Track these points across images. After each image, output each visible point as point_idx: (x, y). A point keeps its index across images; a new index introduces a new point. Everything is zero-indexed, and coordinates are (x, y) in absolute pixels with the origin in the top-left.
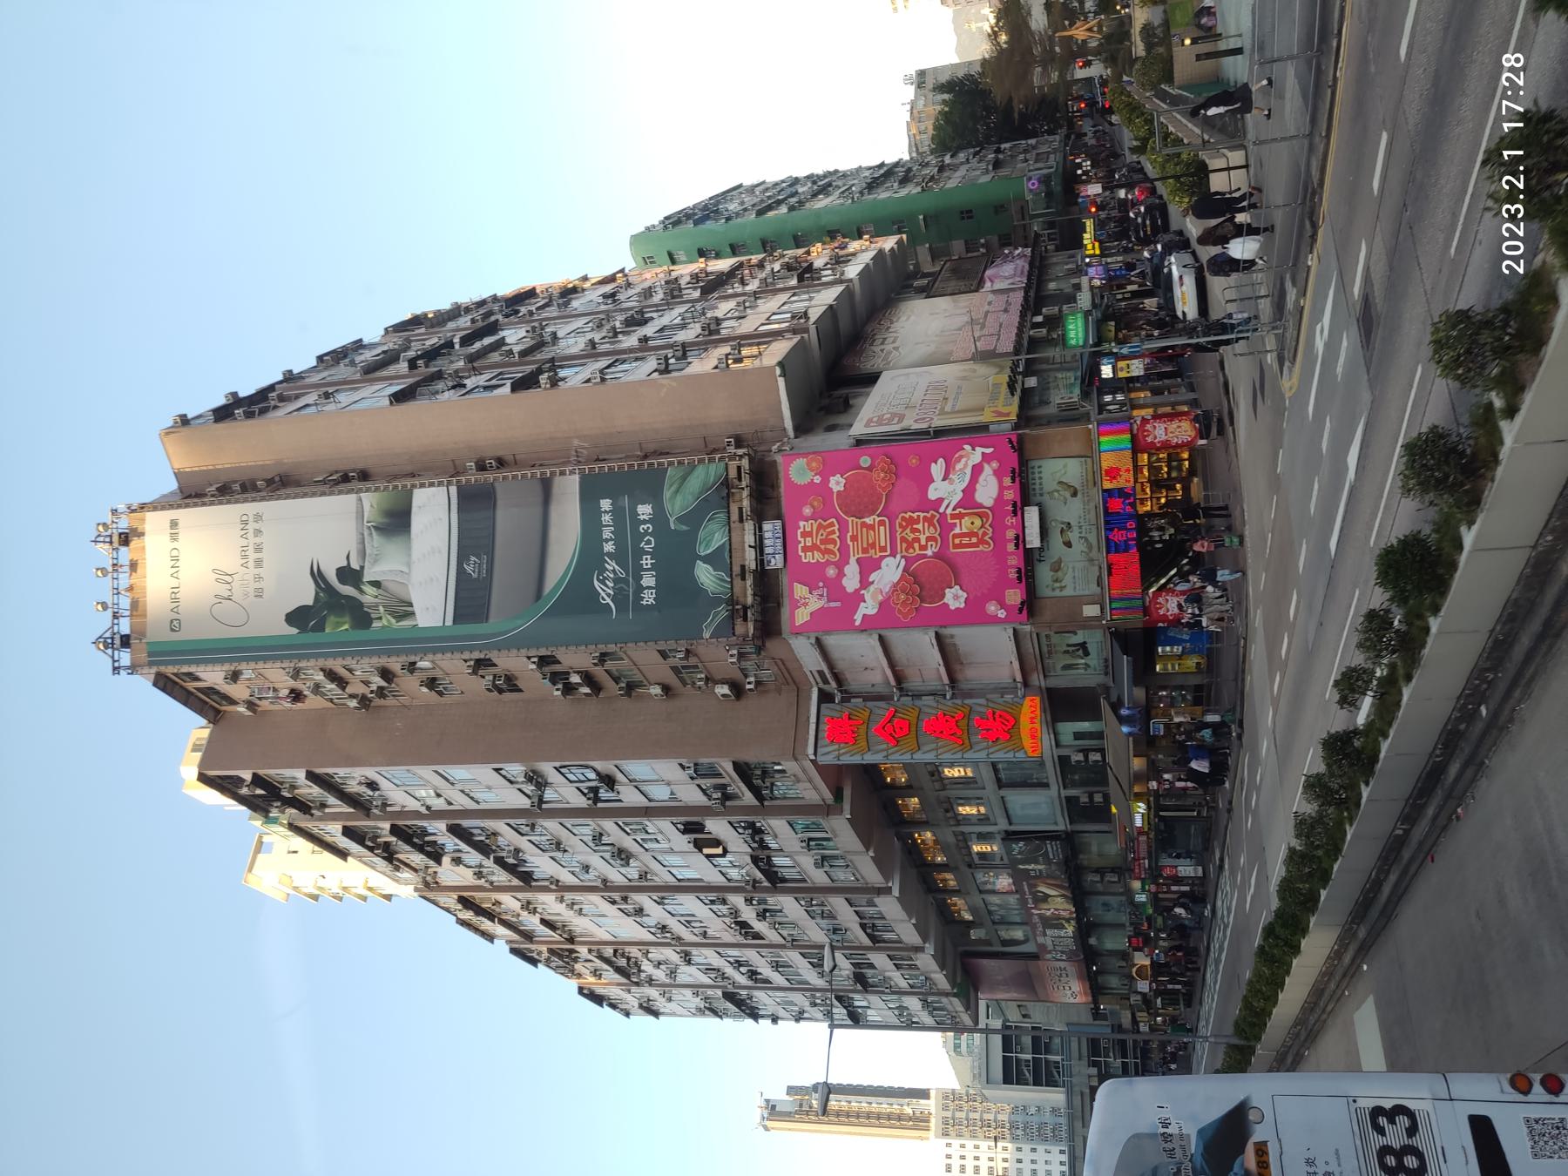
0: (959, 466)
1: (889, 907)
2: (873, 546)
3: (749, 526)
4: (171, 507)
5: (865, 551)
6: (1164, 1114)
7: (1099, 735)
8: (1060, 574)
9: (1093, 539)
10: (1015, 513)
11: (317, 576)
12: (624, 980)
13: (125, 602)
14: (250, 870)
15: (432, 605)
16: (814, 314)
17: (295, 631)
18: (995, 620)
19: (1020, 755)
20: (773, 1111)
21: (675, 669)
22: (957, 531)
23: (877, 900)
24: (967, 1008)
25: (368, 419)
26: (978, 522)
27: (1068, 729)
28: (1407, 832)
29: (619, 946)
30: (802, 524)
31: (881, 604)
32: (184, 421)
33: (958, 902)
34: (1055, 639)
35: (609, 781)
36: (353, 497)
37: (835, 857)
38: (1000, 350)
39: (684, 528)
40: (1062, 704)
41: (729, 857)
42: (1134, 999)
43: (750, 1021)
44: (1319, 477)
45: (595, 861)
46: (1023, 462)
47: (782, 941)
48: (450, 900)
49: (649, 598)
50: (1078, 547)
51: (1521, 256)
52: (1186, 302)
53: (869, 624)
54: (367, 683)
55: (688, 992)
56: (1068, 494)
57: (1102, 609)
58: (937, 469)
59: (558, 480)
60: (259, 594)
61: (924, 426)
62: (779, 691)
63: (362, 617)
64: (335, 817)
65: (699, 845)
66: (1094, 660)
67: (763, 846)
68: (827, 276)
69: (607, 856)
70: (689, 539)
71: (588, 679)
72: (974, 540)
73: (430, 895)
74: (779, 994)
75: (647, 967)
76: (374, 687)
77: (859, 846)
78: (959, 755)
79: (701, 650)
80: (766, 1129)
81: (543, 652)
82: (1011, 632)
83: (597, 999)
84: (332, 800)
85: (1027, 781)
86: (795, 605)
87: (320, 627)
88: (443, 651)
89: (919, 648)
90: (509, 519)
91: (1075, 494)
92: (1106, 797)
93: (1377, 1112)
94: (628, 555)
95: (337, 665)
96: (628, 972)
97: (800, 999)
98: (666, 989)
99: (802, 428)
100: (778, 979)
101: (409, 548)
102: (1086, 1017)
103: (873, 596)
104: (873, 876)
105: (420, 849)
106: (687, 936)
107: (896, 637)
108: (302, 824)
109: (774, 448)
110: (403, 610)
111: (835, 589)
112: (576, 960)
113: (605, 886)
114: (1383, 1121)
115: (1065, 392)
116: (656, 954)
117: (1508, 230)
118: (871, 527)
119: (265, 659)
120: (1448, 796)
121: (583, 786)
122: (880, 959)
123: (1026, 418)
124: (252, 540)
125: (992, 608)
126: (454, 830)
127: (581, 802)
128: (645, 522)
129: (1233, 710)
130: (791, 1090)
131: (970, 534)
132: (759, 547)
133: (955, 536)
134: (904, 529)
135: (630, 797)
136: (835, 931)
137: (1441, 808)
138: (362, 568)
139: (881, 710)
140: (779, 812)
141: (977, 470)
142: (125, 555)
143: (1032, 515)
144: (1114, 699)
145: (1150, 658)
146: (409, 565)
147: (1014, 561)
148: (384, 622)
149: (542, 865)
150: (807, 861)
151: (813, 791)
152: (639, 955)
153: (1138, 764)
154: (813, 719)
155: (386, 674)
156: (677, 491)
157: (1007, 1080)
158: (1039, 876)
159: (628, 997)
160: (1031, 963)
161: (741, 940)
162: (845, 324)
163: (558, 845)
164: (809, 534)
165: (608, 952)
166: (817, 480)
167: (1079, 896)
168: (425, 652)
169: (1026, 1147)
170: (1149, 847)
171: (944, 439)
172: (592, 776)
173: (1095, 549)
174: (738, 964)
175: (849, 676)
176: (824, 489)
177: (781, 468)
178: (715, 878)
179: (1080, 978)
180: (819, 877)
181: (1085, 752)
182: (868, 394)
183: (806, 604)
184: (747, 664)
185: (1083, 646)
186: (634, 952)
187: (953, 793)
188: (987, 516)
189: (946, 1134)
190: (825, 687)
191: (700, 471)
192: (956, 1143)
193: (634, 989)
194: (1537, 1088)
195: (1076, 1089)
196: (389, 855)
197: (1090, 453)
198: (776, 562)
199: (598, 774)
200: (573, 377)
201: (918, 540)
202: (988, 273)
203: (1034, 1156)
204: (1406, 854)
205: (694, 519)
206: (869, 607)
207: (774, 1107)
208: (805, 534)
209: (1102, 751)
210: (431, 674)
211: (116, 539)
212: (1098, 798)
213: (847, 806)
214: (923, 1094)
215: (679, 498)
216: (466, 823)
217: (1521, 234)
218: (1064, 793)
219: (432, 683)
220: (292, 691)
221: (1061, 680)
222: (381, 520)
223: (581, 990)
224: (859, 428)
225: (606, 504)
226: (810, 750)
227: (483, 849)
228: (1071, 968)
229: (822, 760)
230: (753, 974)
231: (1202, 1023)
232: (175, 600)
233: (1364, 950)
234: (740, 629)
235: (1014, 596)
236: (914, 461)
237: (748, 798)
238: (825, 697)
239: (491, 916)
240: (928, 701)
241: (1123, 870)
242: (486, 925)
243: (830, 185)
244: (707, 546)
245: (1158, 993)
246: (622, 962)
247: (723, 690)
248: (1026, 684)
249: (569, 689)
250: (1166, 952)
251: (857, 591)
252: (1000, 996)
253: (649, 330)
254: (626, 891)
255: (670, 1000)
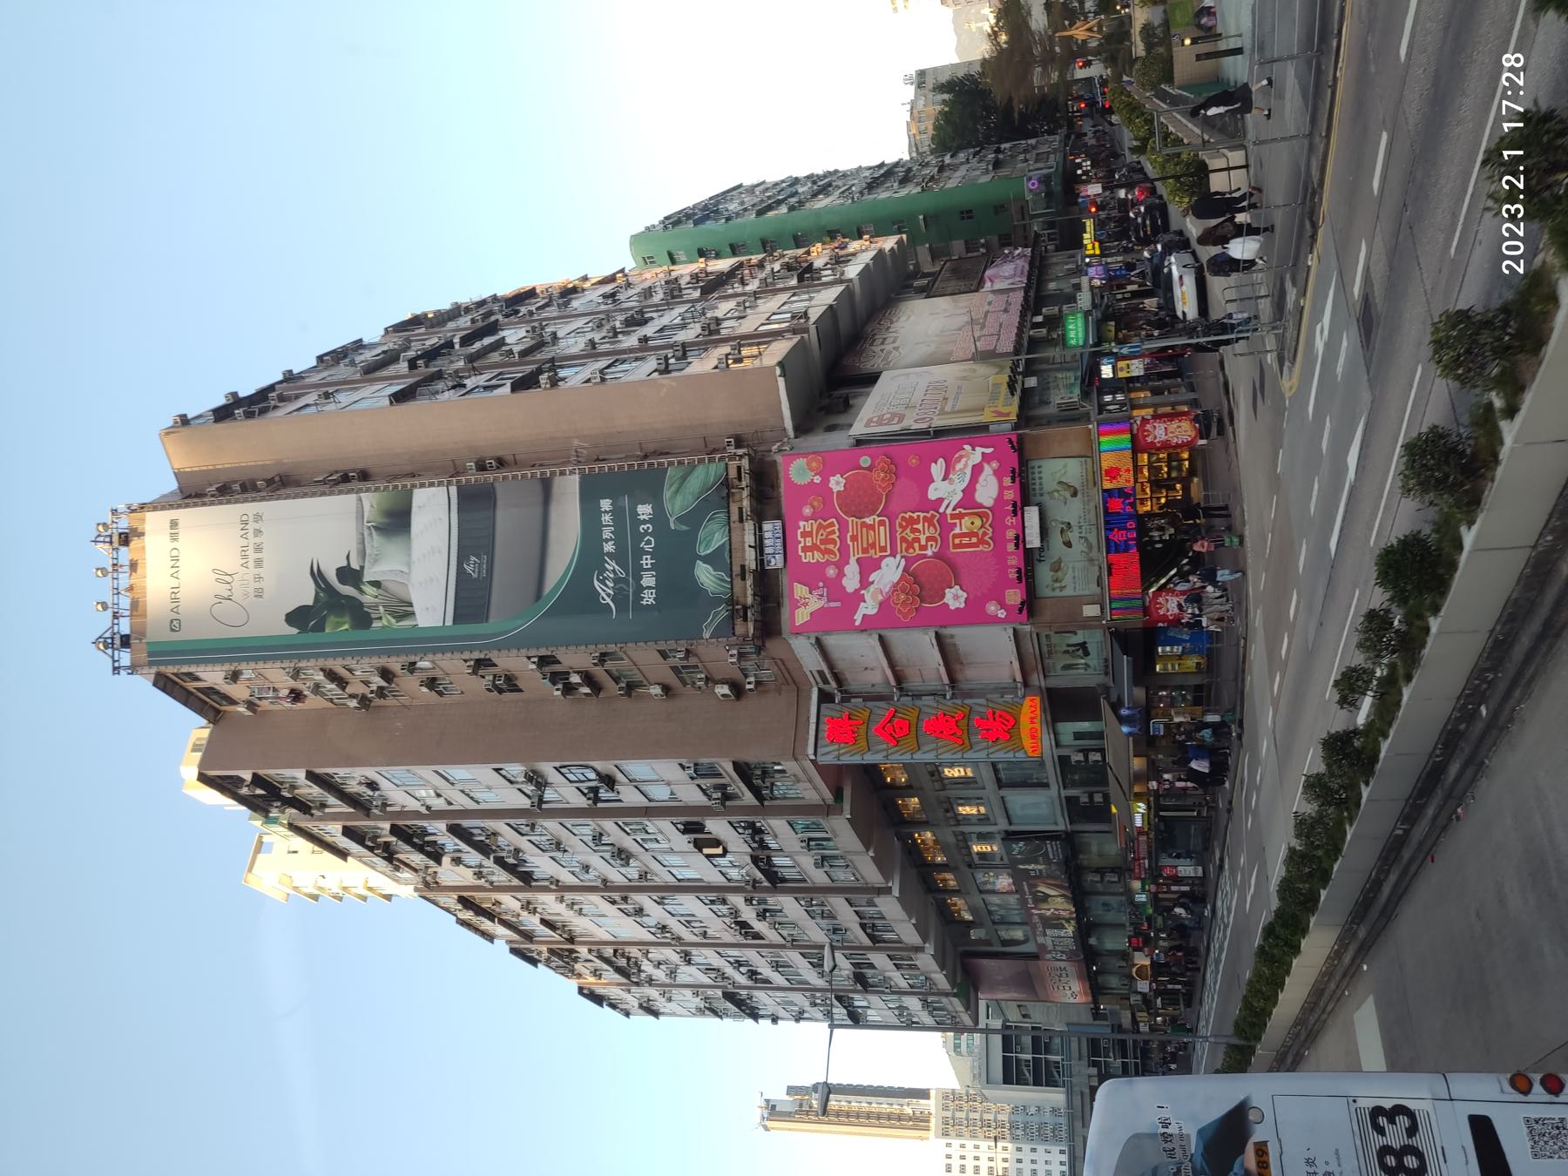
0: (959, 466)
1: (889, 907)
2: (873, 546)
3: (749, 526)
4: (171, 507)
5: (865, 551)
6: (1164, 1114)
7: (1099, 735)
8: (1060, 574)
9: (1093, 539)
10: (1015, 513)
11: (317, 576)
12: (624, 980)
13: (125, 602)
14: (250, 870)
15: (432, 605)
16: (814, 314)
17: (295, 631)
18: (995, 620)
19: (1020, 755)
20: (773, 1111)
21: (675, 669)
22: (957, 531)
23: (877, 900)
24: (967, 1008)
25: (368, 419)
26: (978, 522)
27: (1068, 729)
28: (1407, 832)
29: (619, 946)
30: (802, 524)
31: (881, 604)
32: (184, 421)
33: (958, 902)
34: (1055, 639)
35: (609, 781)
36: (353, 497)
37: (835, 857)
38: (1000, 350)
39: (684, 528)
40: (1062, 704)
41: (729, 857)
42: (1134, 999)
43: (750, 1021)
44: (1319, 477)
45: (595, 861)
46: (1023, 462)
47: (782, 941)
48: (450, 900)
49: (649, 598)
50: (1078, 547)
51: (1521, 256)
52: (1186, 302)
53: (869, 624)
54: (367, 683)
55: (688, 992)
56: (1068, 494)
57: (1102, 609)
58: (937, 469)
59: (558, 480)
60: (259, 594)
61: (924, 426)
62: (779, 691)
63: (362, 617)
64: (335, 817)
65: (699, 845)
66: (1094, 660)
67: (763, 846)
68: (827, 276)
69: (607, 856)
70: (689, 539)
71: (588, 679)
72: (974, 540)
73: (430, 895)
74: (779, 994)
75: (647, 967)
76: (374, 687)
77: (859, 846)
78: (959, 755)
79: (701, 650)
80: (766, 1129)
81: (543, 652)
82: (1011, 632)
83: (597, 999)
84: (332, 800)
85: (1027, 781)
86: (795, 605)
87: (320, 627)
88: (443, 651)
89: (919, 648)
90: (509, 519)
91: (1075, 494)
92: (1106, 797)
93: (1377, 1112)
94: (628, 555)
95: (337, 665)
96: (628, 972)
97: (800, 999)
98: (666, 989)
99: (802, 428)
100: (778, 979)
101: (409, 548)
102: (1086, 1017)
103: (873, 596)
104: (873, 876)
105: (420, 849)
106: (687, 936)
107: (896, 637)
108: (302, 824)
109: (774, 448)
110: (403, 610)
111: (835, 589)
112: (576, 960)
113: (605, 886)
114: (1383, 1121)
115: (1065, 392)
116: (656, 954)
117: (1508, 230)
118: (871, 527)
119: (265, 659)
120: (1448, 796)
121: (583, 786)
122: (880, 959)
123: (1026, 418)
124: (252, 540)
125: (992, 608)
126: (454, 830)
127: (581, 802)
128: (645, 522)
129: (1233, 710)
130: (791, 1090)
131: (970, 534)
132: (759, 547)
133: (955, 536)
134: (904, 529)
135: (630, 797)
136: (835, 931)
137: (1441, 808)
138: (362, 568)
139: (881, 710)
140: (779, 812)
141: (977, 470)
142: (125, 555)
143: (1032, 515)
144: (1114, 699)
145: (1150, 658)
146: (409, 565)
147: (1014, 561)
148: (384, 622)
149: (542, 865)
150: (807, 861)
151: (813, 791)
152: (639, 955)
153: (1138, 764)
154: (813, 719)
155: (386, 674)
156: (677, 491)
157: (1007, 1080)
158: (1039, 876)
159: (628, 997)
160: (1031, 963)
161: (741, 940)
162: (845, 324)
163: (558, 845)
164: (809, 534)
165: (608, 952)
166: (817, 480)
167: (1079, 896)
168: (425, 652)
169: (1026, 1147)
170: (1149, 847)
171: (944, 439)
172: (592, 776)
173: (1095, 549)
174: (738, 964)
175: (849, 676)
176: (824, 489)
177: (781, 468)
178: (715, 878)
179: (1080, 978)
180: (819, 877)
181: (1085, 752)
182: (868, 394)
183: (806, 604)
184: (747, 664)
185: (1083, 646)
186: (634, 952)
187: (953, 793)
188: (987, 516)
189: (946, 1134)
190: (825, 687)
191: (700, 471)
192: (956, 1143)
193: (634, 989)
194: (1537, 1088)
195: (1076, 1089)
196: (389, 855)
197: (1090, 453)
198: (776, 562)
199: (598, 774)
200: (573, 377)
201: (918, 540)
202: (988, 273)
203: (1034, 1156)
204: (1406, 854)
205: (694, 519)
206: (869, 607)
207: (774, 1107)
208: (805, 534)
209: (1102, 751)
210: (431, 674)
211: (116, 539)
212: (1098, 798)
213: (847, 806)
214: (923, 1094)
215: (679, 498)
216: (466, 823)
217: (1521, 234)
218: (1064, 793)
219: (432, 683)
220: (292, 691)
221: (1061, 680)
222: (381, 520)
223: (581, 990)
224: (859, 428)
225: (606, 504)
226: (810, 750)
227: (483, 849)
228: (1071, 968)
229: (822, 760)
230: (753, 974)
231: (1202, 1023)
232: (175, 600)
233: (1364, 950)
234: (740, 629)
235: (1014, 596)
236: (914, 461)
237: (748, 798)
238: (825, 697)
239: (491, 916)
240: (928, 701)
241: (1123, 870)
242: (486, 925)
243: (830, 185)
244: (707, 546)
245: (1158, 993)
246: (622, 962)
247: (723, 690)
248: (1026, 684)
249: (569, 689)
250: (1166, 952)
251: (857, 591)
252: (1000, 996)
253: (649, 330)
254: (626, 891)
255: (670, 1000)
